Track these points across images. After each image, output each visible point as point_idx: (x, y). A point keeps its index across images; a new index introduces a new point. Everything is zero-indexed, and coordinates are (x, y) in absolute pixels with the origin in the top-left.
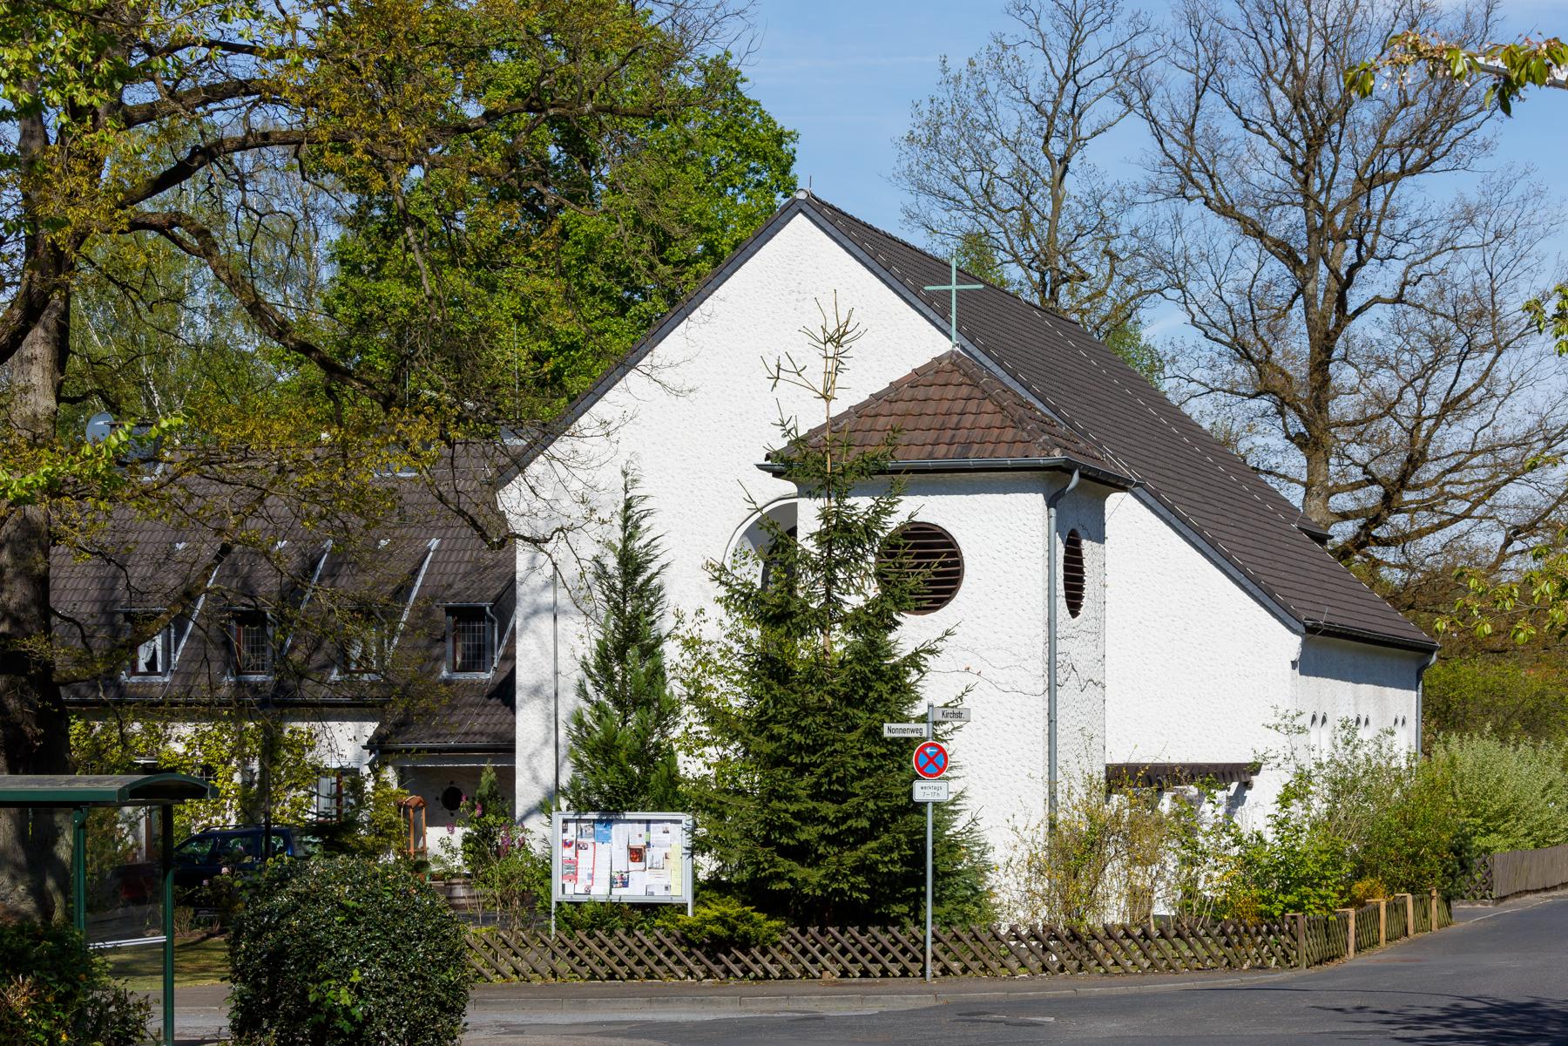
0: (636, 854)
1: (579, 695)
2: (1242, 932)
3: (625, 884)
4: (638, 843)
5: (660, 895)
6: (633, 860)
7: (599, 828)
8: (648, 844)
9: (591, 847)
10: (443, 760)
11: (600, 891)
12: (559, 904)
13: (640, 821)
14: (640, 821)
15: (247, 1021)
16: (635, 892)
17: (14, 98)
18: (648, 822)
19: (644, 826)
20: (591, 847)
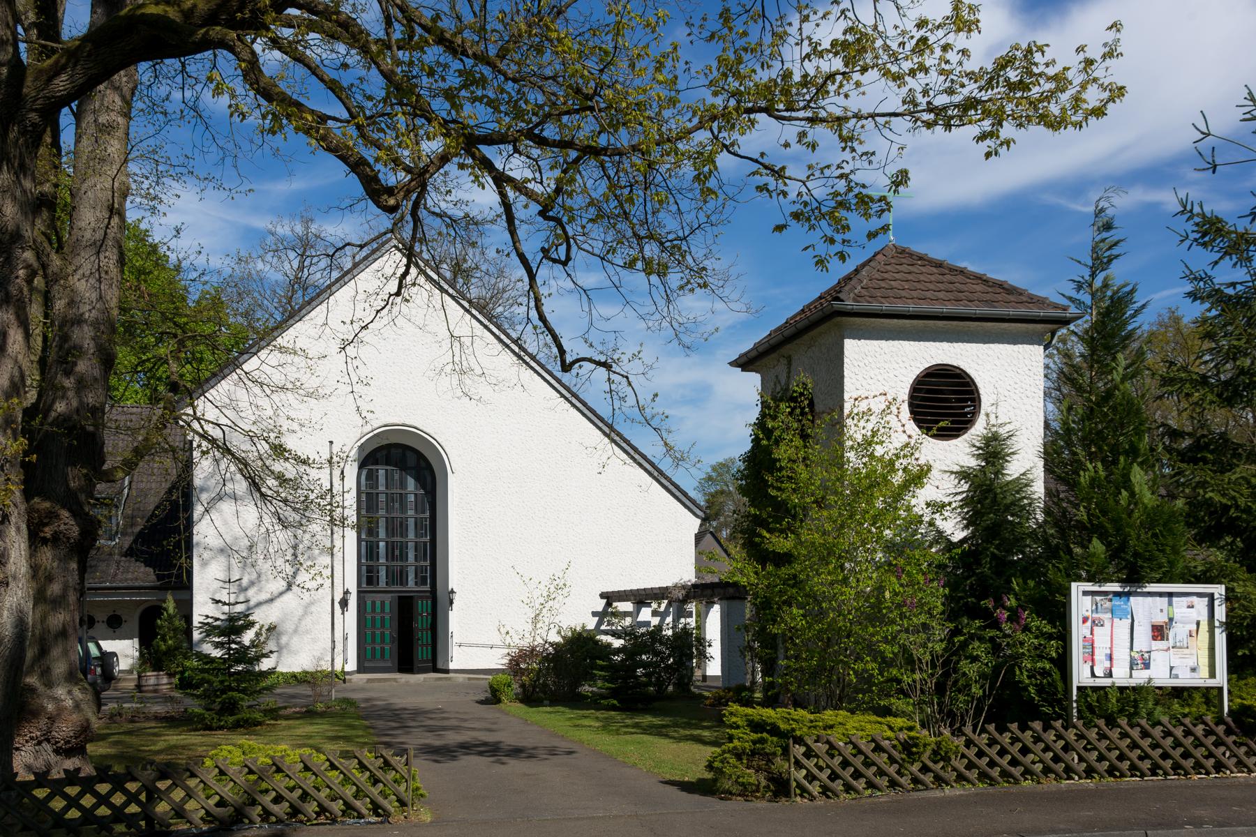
0: (1159, 632)
1: (928, 128)
2: (871, 486)
3: (1147, 666)
4: (1161, 619)
5: (1185, 679)
6: (1154, 638)
7: (1117, 602)
8: (1171, 620)
9: (1108, 624)
10: (96, 595)
11: (1122, 676)
12: (1079, 688)
13: (1161, 595)
14: (1161, 595)
15: (1249, 403)
16: (1159, 675)
17: (785, 184)
18: (1170, 595)
19: (1166, 599)
20: (1108, 624)
